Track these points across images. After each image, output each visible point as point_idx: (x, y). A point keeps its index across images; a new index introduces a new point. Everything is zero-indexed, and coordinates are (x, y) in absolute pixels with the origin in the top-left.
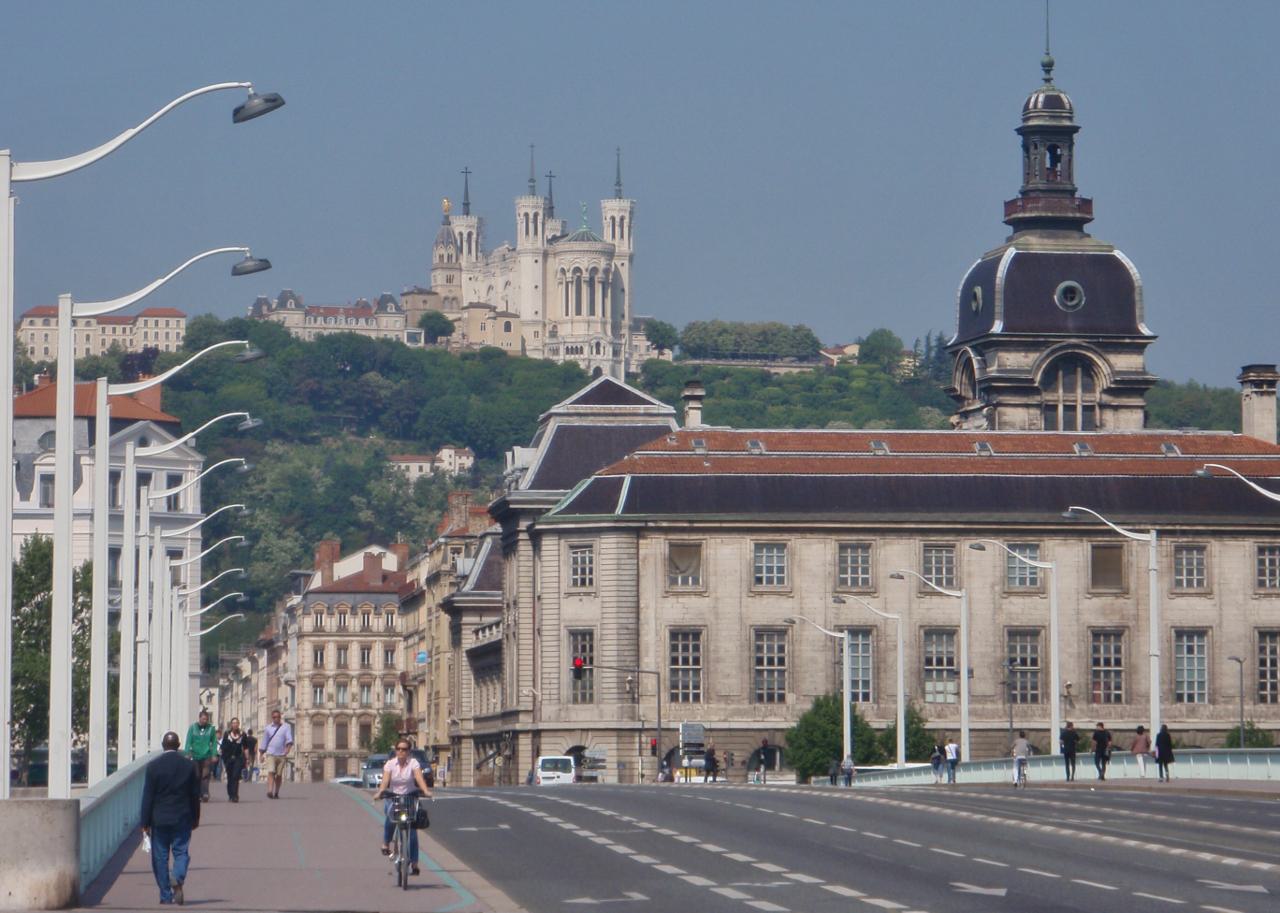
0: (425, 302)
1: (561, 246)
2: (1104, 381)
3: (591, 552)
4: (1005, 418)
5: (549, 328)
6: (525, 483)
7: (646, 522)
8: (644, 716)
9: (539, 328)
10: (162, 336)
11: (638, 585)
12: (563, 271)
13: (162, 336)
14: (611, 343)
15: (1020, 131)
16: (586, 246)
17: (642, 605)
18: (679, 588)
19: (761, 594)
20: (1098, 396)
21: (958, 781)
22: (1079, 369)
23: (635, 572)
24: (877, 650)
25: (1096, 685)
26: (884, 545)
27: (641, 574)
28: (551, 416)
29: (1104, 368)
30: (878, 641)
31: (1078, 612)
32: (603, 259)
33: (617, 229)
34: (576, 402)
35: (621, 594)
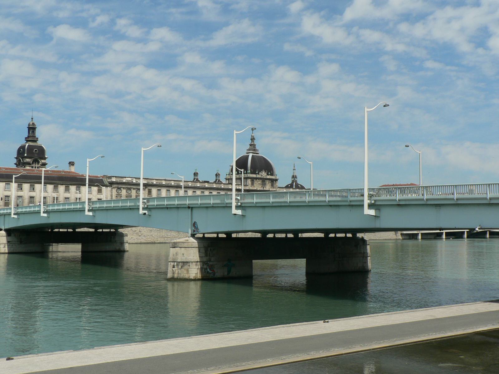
2: (40, 164)
15: (28, 128)
19: (6, 191)
20: (39, 165)
21: (273, 234)
22: (37, 163)
24: (23, 199)
29: (41, 162)
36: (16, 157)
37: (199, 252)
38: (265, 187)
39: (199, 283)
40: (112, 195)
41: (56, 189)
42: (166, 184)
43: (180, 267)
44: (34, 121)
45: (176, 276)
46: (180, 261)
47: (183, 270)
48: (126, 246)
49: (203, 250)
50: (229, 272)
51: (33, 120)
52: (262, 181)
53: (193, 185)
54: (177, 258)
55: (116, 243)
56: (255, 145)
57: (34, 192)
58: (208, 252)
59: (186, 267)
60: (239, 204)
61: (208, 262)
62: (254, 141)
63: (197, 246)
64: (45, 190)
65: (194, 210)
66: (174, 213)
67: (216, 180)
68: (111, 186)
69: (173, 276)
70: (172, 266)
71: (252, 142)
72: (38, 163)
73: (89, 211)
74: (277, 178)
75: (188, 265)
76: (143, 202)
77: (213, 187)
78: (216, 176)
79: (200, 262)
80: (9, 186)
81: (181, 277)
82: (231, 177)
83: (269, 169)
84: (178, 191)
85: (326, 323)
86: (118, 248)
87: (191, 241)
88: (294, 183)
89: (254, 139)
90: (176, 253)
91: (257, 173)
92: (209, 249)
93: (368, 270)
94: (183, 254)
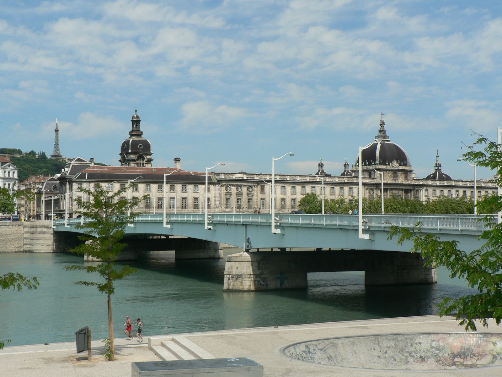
2: (146, 160)
4: (131, 165)
6: (68, 174)
15: (132, 121)
18: (159, 191)
20: (144, 162)
22: (142, 159)
25: (158, 206)
28: (71, 163)
29: (146, 158)
31: (156, 195)
34: (75, 161)
36: (120, 153)
37: (252, 265)
38: (397, 180)
39: (252, 294)
40: (221, 193)
41: (160, 189)
42: (281, 180)
43: (235, 279)
44: (138, 113)
45: (231, 287)
46: (235, 274)
47: (237, 282)
48: (221, 253)
49: (256, 264)
50: (282, 284)
51: (137, 112)
52: (393, 173)
53: (312, 180)
54: (232, 271)
55: (210, 250)
56: (385, 131)
57: (137, 193)
58: (261, 266)
59: (240, 279)
60: (278, 224)
61: (261, 275)
62: (383, 127)
63: (250, 260)
64: (149, 190)
65: (248, 228)
66: (233, 228)
67: (345, 171)
68: (220, 184)
69: (229, 288)
70: (227, 279)
71: (382, 128)
72: (143, 159)
73: (167, 223)
74: (412, 169)
75: (242, 277)
76: (208, 218)
77: (335, 181)
78: (344, 166)
79: (253, 275)
80: (111, 186)
81: (236, 289)
82: (357, 169)
83: (401, 158)
84: (295, 187)
85: (276, 328)
86: (212, 255)
87: (244, 256)
88: (438, 173)
89: (384, 124)
90: (231, 267)
91: (387, 163)
92: (262, 263)
93: (433, 282)
94: (237, 268)
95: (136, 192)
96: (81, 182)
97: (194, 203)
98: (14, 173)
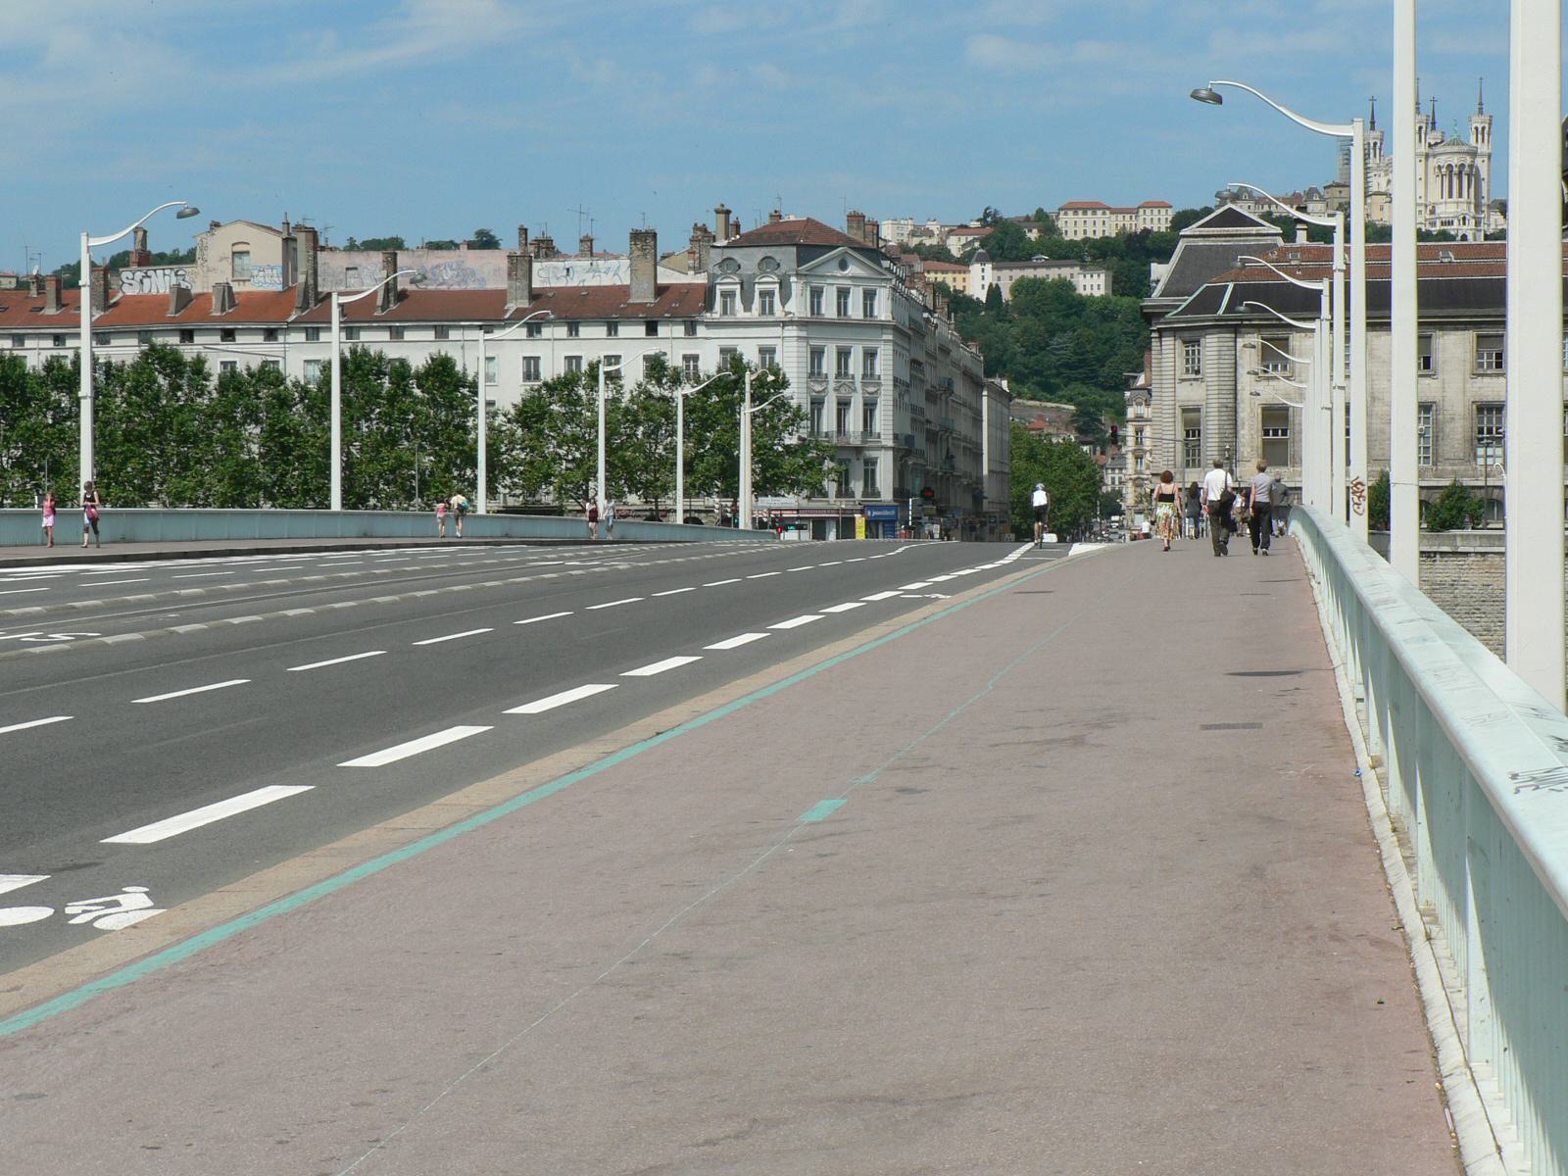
0: (1340, 192)
1: (1439, 149)
3: (1199, 345)
5: (1430, 208)
7: (1242, 320)
8: (1241, 477)
9: (1422, 208)
10: (1156, 221)
11: (1236, 372)
12: (1440, 167)
13: (1156, 221)
14: (1474, 218)
16: (1456, 149)
17: (1239, 388)
23: (1233, 361)
24: (1436, 422)
26: (1443, 336)
27: (1238, 362)
30: (1437, 415)
32: (1468, 158)
33: (1480, 136)
35: (1222, 379)
95: (1490, 375)
96: (1197, 333)
97: (1266, 433)
98: (869, 296)
